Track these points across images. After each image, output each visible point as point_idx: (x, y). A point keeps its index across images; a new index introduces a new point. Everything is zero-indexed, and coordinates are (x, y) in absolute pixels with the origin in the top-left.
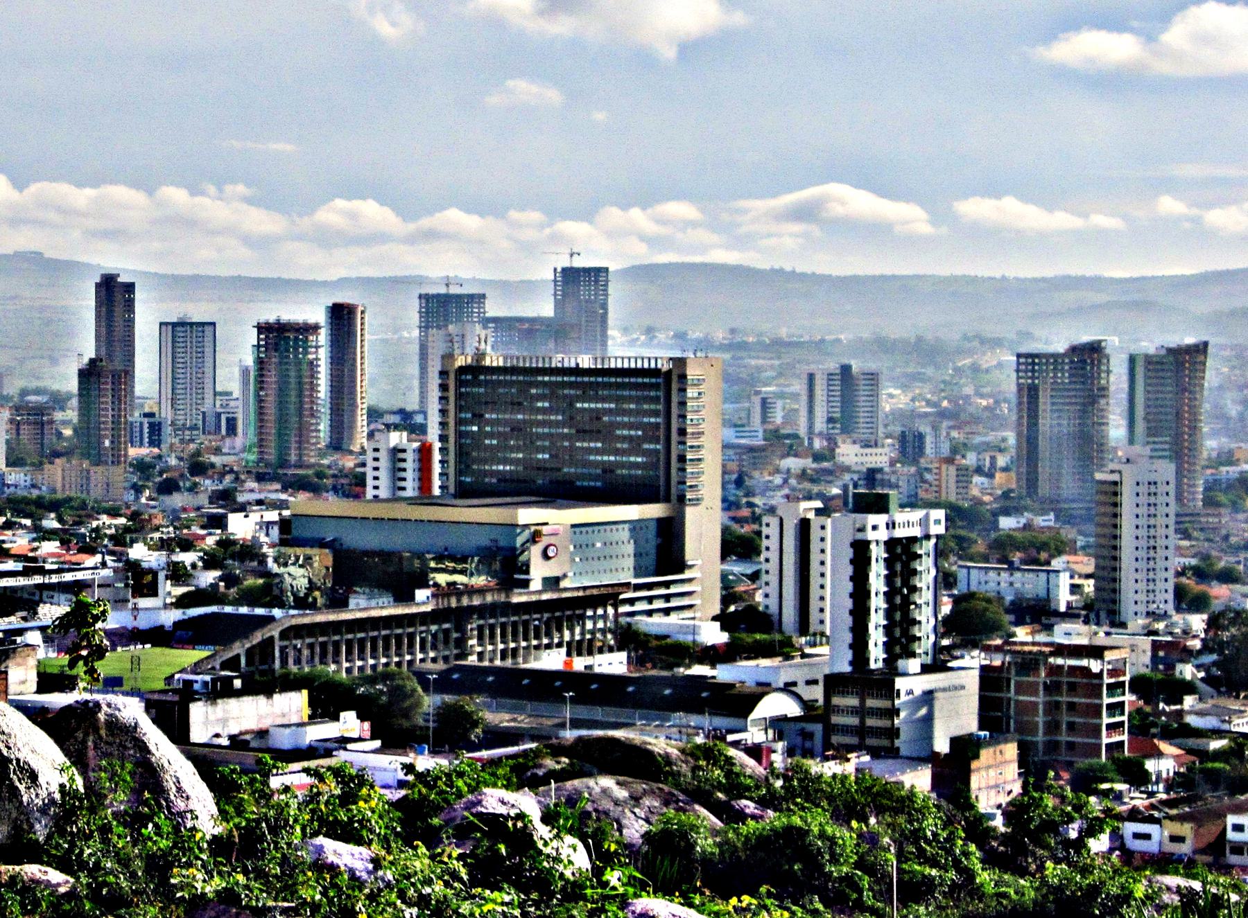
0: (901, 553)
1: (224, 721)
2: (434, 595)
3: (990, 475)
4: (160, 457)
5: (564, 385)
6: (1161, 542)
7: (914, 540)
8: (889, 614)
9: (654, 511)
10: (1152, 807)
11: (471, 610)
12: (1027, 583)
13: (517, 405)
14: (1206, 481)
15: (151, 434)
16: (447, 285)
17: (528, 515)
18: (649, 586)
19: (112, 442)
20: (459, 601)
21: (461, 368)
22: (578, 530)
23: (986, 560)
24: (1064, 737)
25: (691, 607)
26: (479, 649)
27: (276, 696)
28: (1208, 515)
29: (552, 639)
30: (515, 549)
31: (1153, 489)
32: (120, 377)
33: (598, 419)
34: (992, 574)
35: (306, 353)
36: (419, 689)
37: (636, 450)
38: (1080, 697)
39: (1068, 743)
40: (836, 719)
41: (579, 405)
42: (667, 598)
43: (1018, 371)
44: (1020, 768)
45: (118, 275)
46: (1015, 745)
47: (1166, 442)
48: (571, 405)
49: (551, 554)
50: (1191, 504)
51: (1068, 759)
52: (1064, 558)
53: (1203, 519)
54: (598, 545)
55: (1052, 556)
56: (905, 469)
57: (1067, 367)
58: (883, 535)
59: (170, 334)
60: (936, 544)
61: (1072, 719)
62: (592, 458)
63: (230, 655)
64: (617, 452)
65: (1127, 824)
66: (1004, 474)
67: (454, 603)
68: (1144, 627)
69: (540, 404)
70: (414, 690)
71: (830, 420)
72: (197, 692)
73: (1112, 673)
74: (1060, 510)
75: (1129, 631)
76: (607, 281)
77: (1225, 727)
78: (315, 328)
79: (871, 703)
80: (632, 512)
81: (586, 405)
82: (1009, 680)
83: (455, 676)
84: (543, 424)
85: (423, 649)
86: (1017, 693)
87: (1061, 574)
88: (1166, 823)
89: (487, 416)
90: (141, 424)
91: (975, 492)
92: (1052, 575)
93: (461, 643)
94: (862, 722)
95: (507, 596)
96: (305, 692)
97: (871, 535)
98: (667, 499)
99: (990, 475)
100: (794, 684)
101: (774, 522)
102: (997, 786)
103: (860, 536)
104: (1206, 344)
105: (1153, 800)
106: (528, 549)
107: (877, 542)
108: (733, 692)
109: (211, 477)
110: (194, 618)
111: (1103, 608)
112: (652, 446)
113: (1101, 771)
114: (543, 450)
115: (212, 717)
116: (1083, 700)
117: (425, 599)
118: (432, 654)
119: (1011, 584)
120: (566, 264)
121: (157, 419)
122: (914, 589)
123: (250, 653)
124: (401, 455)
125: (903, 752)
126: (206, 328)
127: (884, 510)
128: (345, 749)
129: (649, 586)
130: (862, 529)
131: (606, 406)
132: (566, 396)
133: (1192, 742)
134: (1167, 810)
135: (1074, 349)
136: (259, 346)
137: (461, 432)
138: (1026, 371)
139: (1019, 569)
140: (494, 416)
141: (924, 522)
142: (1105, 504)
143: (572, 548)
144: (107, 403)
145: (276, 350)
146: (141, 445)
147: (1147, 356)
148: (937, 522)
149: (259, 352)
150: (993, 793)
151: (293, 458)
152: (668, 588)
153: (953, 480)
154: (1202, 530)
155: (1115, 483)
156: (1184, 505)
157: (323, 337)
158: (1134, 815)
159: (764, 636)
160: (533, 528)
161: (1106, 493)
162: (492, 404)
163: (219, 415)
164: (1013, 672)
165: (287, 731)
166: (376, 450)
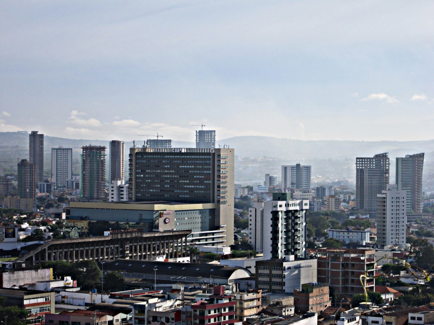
0: (291, 215)
1: (17, 280)
2: (111, 233)
3: (348, 203)
4: (48, 196)
5: (175, 159)
6: (401, 220)
7: (296, 211)
8: (286, 239)
9: (209, 206)
10: (380, 311)
11: (127, 239)
12: (354, 237)
13: (158, 167)
14: (424, 204)
15: (47, 188)
16: (157, 137)
17: (157, 207)
18: (206, 234)
19: (30, 190)
20: (121, 236)
21: (137, 153)
22: (178, 213)
23: (341, 229)
24: (350, 285)
25: (222, 242)
26: (130, 255)
27: (39, 271)
28: (424, 215)
29: (160, 251)
30: (153, 220)
31: (398, 200)
32: (33, 166)
33: (188, 172)
34: (341, 233)
35: (100, 157)
36: (98, 268)
37: (201, 183)
38: (355, 269)
39: (351, 287)
40: (260, 279)
41: (180, 167)
42: (213, 239)
43: (357, 164)
44: (330, 296)
45: (38, 132)
46: (328, 287)
47: (409, 189)
48: (178, 166)
49: (167, 222)
50: (418, 211)
51: (351, 294)
52: (369, 229)
53: (423, 217)
54: (186, 219)
55: (365, 228)
56: (318, 200)
57: (374, 163)
58: (284, 209)
59: (55, 153)
60: (306, 213)
61: (353, 278)
62: (185, 186)
63: (30, 256)
64: (195, 184)
65: (369, 317)
66: (353, 202)
67: (119, 237)
68: (390, 248)
69: (166, 166)
70: (96, 268)
71: (292, 184)
72: (7, 269)
73: (368, 260)
74: (371, 214)
75: (385, 250)
76: (215, 135)
77: (416, 282)
78: (104, 149)
79: (274, 272)
80: (199, 206)
81: (183, 167)
82: (328, 263)
83: (117, 264)
84: (166, 174)
85: (107, 255)
86: (331, 268)
87: (367, 233)
88: (384, 316)
89: (147, 171)
90: (44, 185)
91: (342, 208)
92: (363, 233)
93: (123, 252)
94: (271, 280)
95: (141, 234)
96: (51, 269)
97: (279, 209)
98: (213, 202)
99: (348, 203)
100: (250, 267)
101: (253, 210)
102: (320, 303)
103: (274, 209)
104: (423, 154)
105: (381, 308)
106: (158, 219)
107: (282, 211)
108: (223, 269)
109: (66, 203)
110: (29, 245)
111: (380, 244)
112: (208, 182)
113: (363, 298)
114: (167, 183)
115: (12, 279)
116: (357, 271)
117: (108, 235)
118: (111, 257)
119: (348, 237)
120: (200, 129)
121: (49, 183)
122: (296, 230)
123: (37, 255)
124: (122, 189)
125: (286, 291)
126: (69, 151)
127: (285, 199)
128: (65, 291)
129: (206, 234)
130: (275, 206)
131: (190, 167)
132: (175, 163)
133: (401, 288)
134: (386, 312)
135: (376, 156)
136: (83, 155)
137: (137, 177)
138: (359, 164)
139: (351, 231)
140: (149, 171)
141: (301, 204)
142: (380, 206)
143: (175, 220)
144: (28, 176)
145: (89, 157)
146: (44, 192)
147: (402, 158)
148: (306, 204)
149: (83, 157)
150: (319, 306)
151: (95, 196)
152: (214, 235)
153: (333, 203)
154: (422, 220)
155: (384, 198)
156: (416, 212)
157: (108, 151)
158: (373, 314)
159: (245, 251)
160: (160, 212)
161: (380, 202)
162: (148, 167)
163: (73, 182)
164: (330, 260)
165: (43, 284)
166: (112, 187)
